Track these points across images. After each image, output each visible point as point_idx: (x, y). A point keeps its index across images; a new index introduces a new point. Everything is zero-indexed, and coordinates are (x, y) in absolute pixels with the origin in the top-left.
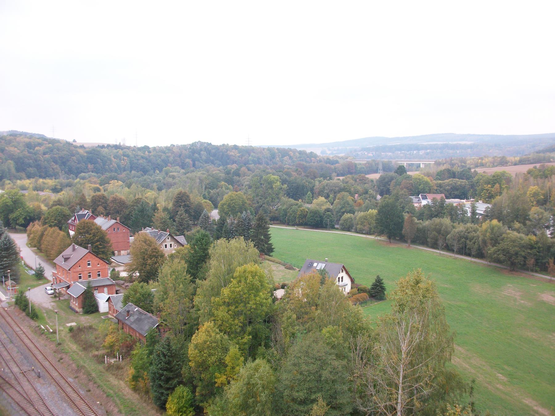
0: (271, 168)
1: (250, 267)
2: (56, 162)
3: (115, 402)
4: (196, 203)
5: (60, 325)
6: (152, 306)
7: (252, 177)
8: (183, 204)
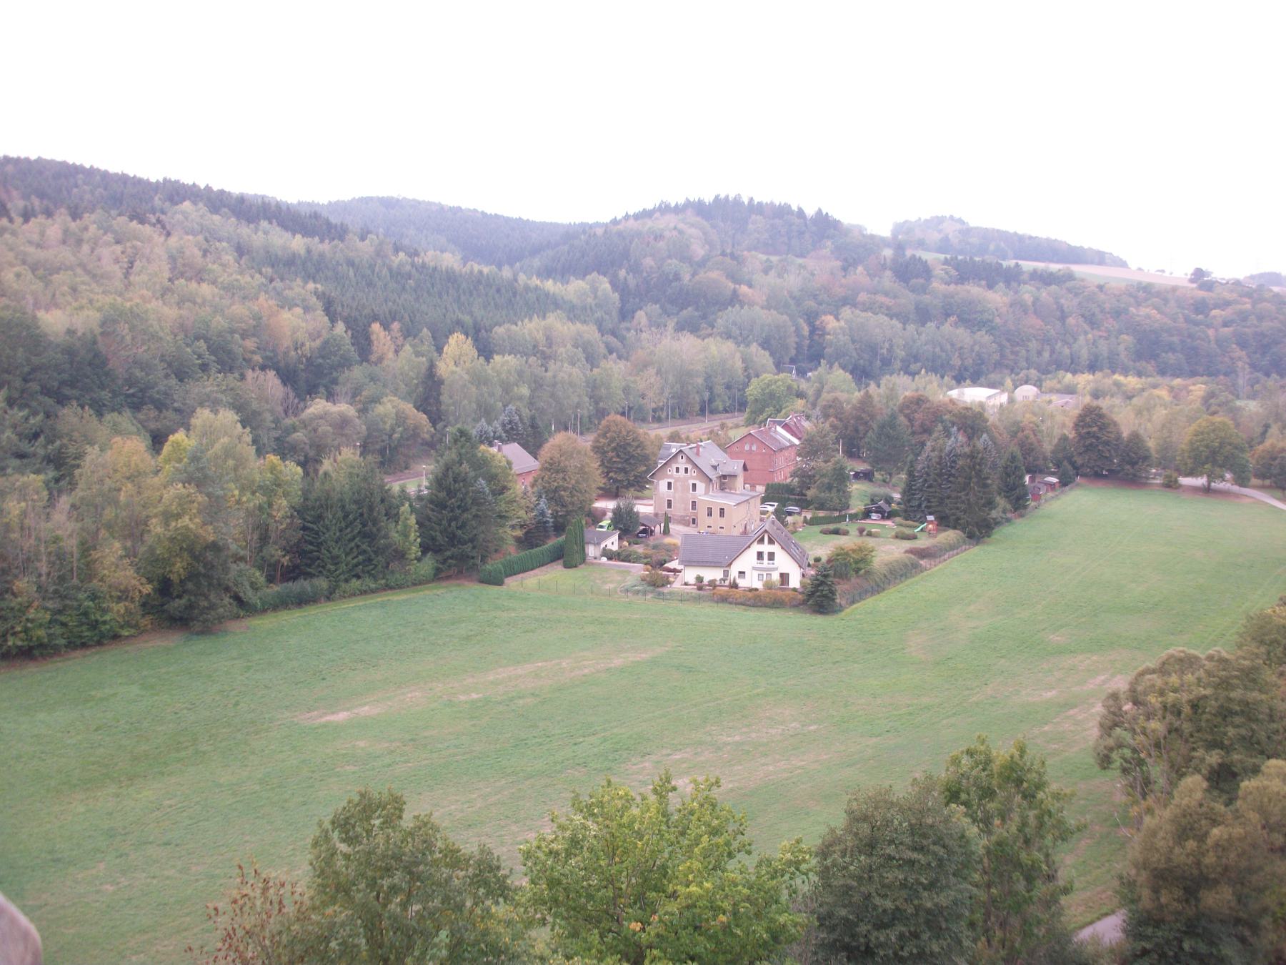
2: (1243, 345)
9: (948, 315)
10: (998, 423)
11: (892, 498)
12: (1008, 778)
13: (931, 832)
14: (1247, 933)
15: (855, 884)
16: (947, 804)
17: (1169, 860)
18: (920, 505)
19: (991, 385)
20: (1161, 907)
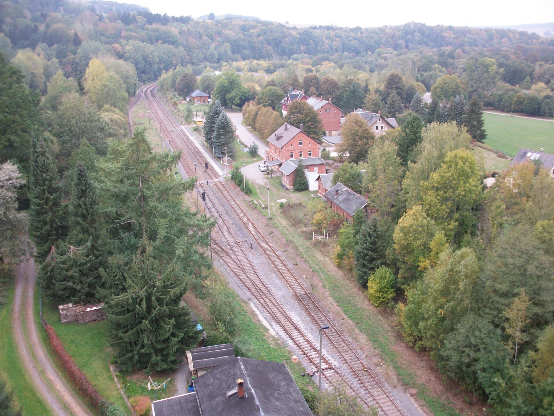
0: (488, 51)
1: (461, 152)
2: (269, 44)
3: (319, 277)
4: (409, 85)
5: (271, 201)
6: (361, 187)
7: (468, 60)
8: (395, 86)
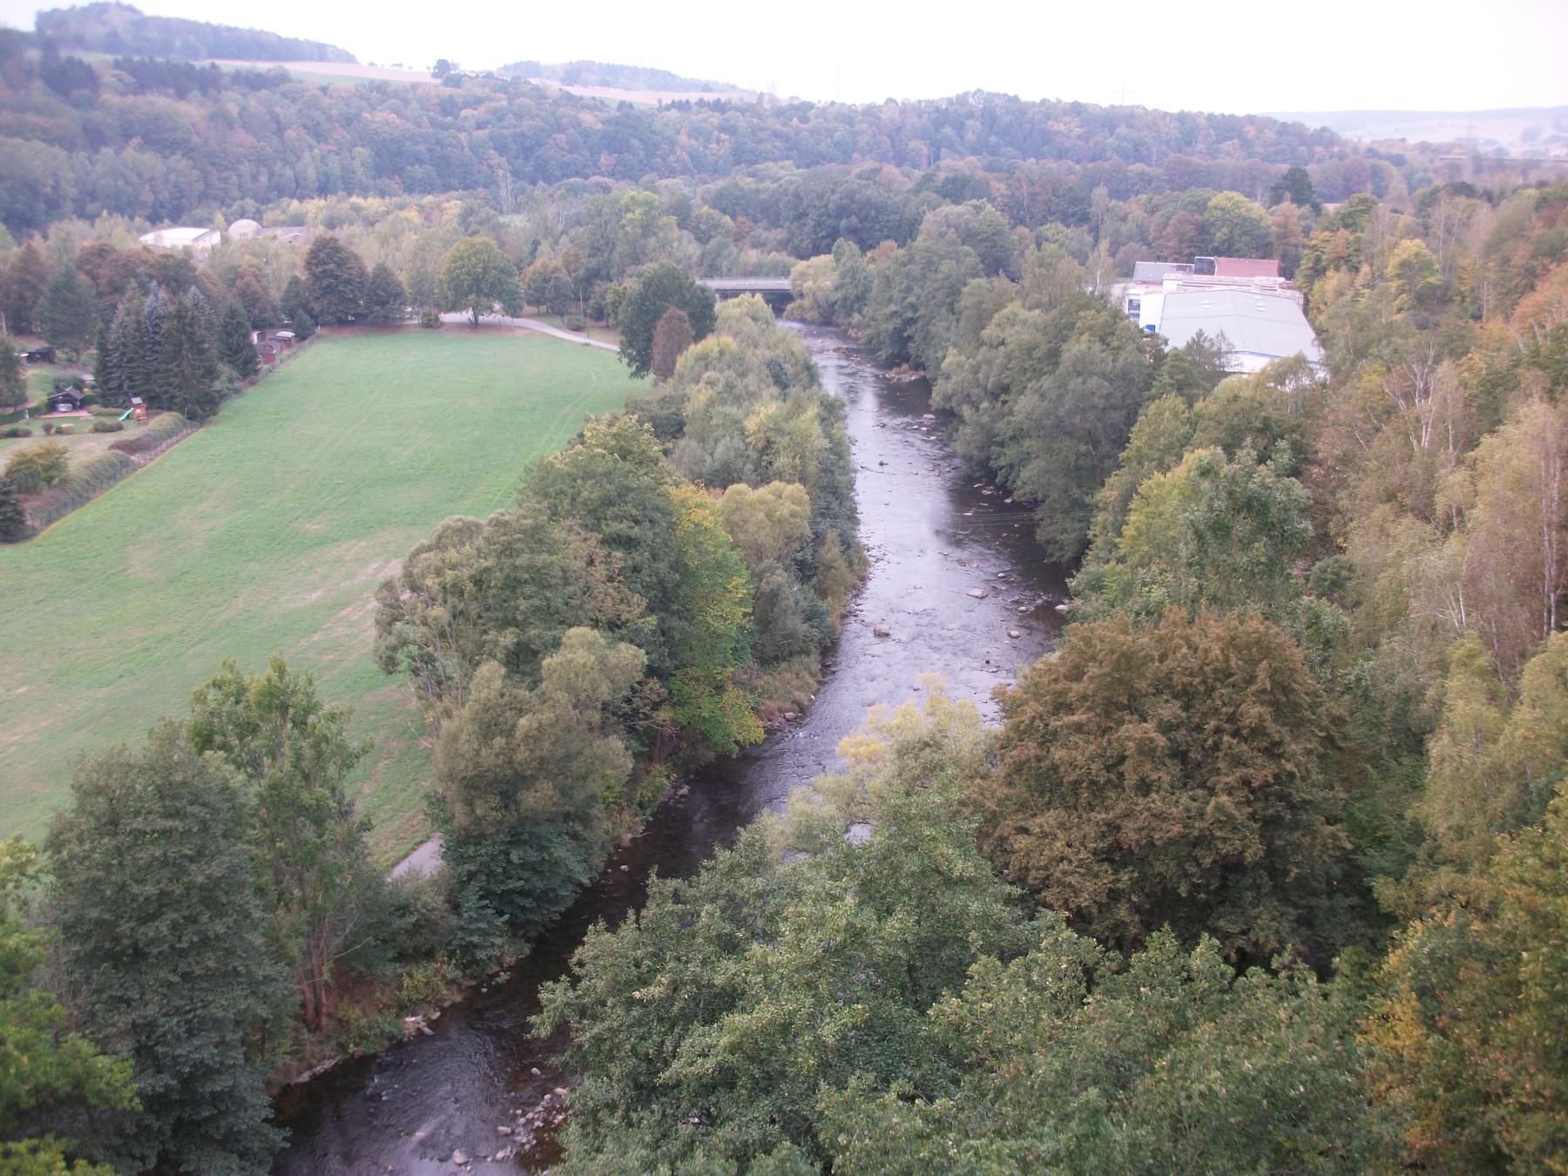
2: (501, 149)
9: (128, 136)
10: (210, 271)
11: (83, 381)
12: (270, 706)
13: (184, 791)
14: (579, 828)
15: (101, 874)
16: (200, 753)
17: (478, 765)
18: (120, 387)
19: (198, 224)
20: (478, 821)
